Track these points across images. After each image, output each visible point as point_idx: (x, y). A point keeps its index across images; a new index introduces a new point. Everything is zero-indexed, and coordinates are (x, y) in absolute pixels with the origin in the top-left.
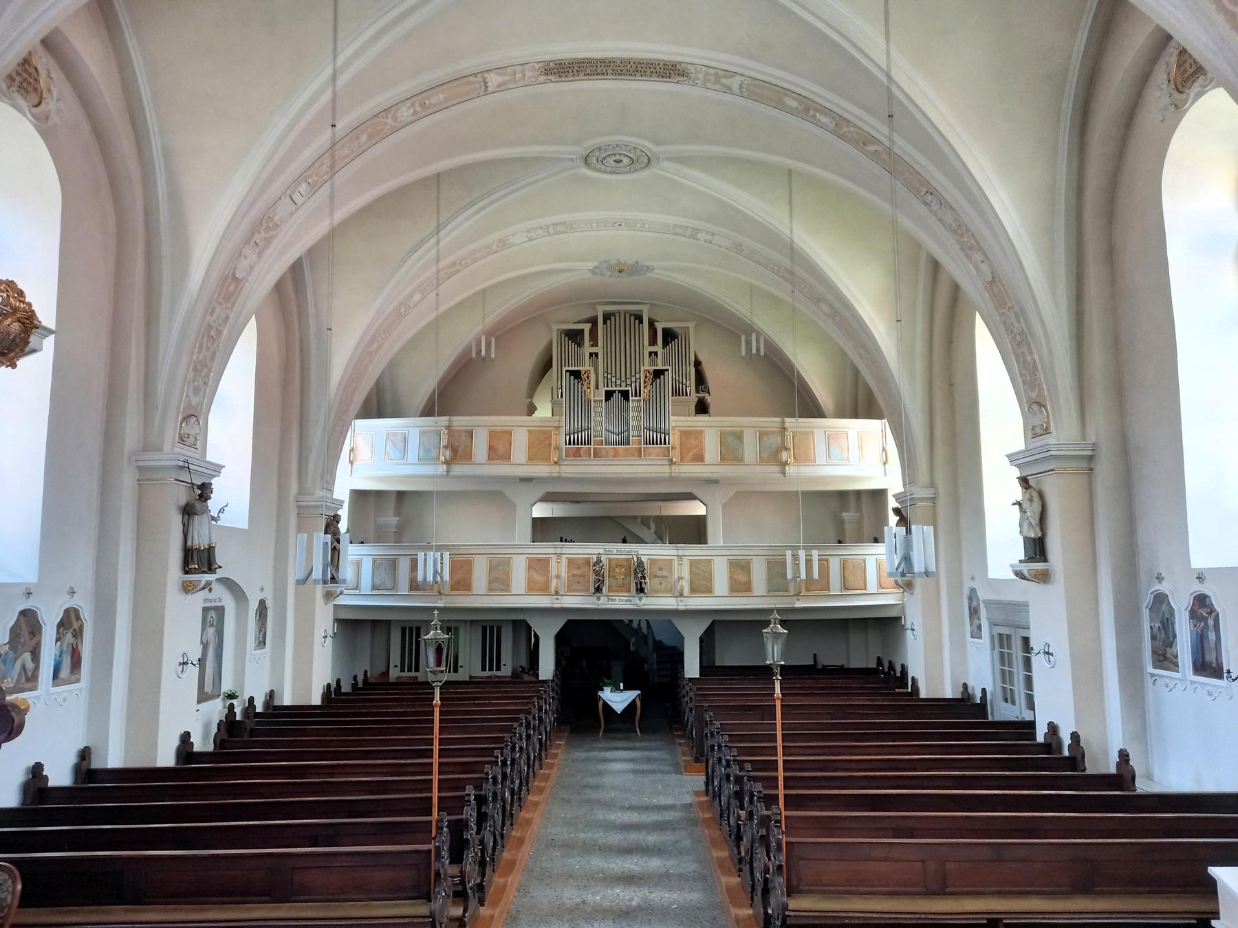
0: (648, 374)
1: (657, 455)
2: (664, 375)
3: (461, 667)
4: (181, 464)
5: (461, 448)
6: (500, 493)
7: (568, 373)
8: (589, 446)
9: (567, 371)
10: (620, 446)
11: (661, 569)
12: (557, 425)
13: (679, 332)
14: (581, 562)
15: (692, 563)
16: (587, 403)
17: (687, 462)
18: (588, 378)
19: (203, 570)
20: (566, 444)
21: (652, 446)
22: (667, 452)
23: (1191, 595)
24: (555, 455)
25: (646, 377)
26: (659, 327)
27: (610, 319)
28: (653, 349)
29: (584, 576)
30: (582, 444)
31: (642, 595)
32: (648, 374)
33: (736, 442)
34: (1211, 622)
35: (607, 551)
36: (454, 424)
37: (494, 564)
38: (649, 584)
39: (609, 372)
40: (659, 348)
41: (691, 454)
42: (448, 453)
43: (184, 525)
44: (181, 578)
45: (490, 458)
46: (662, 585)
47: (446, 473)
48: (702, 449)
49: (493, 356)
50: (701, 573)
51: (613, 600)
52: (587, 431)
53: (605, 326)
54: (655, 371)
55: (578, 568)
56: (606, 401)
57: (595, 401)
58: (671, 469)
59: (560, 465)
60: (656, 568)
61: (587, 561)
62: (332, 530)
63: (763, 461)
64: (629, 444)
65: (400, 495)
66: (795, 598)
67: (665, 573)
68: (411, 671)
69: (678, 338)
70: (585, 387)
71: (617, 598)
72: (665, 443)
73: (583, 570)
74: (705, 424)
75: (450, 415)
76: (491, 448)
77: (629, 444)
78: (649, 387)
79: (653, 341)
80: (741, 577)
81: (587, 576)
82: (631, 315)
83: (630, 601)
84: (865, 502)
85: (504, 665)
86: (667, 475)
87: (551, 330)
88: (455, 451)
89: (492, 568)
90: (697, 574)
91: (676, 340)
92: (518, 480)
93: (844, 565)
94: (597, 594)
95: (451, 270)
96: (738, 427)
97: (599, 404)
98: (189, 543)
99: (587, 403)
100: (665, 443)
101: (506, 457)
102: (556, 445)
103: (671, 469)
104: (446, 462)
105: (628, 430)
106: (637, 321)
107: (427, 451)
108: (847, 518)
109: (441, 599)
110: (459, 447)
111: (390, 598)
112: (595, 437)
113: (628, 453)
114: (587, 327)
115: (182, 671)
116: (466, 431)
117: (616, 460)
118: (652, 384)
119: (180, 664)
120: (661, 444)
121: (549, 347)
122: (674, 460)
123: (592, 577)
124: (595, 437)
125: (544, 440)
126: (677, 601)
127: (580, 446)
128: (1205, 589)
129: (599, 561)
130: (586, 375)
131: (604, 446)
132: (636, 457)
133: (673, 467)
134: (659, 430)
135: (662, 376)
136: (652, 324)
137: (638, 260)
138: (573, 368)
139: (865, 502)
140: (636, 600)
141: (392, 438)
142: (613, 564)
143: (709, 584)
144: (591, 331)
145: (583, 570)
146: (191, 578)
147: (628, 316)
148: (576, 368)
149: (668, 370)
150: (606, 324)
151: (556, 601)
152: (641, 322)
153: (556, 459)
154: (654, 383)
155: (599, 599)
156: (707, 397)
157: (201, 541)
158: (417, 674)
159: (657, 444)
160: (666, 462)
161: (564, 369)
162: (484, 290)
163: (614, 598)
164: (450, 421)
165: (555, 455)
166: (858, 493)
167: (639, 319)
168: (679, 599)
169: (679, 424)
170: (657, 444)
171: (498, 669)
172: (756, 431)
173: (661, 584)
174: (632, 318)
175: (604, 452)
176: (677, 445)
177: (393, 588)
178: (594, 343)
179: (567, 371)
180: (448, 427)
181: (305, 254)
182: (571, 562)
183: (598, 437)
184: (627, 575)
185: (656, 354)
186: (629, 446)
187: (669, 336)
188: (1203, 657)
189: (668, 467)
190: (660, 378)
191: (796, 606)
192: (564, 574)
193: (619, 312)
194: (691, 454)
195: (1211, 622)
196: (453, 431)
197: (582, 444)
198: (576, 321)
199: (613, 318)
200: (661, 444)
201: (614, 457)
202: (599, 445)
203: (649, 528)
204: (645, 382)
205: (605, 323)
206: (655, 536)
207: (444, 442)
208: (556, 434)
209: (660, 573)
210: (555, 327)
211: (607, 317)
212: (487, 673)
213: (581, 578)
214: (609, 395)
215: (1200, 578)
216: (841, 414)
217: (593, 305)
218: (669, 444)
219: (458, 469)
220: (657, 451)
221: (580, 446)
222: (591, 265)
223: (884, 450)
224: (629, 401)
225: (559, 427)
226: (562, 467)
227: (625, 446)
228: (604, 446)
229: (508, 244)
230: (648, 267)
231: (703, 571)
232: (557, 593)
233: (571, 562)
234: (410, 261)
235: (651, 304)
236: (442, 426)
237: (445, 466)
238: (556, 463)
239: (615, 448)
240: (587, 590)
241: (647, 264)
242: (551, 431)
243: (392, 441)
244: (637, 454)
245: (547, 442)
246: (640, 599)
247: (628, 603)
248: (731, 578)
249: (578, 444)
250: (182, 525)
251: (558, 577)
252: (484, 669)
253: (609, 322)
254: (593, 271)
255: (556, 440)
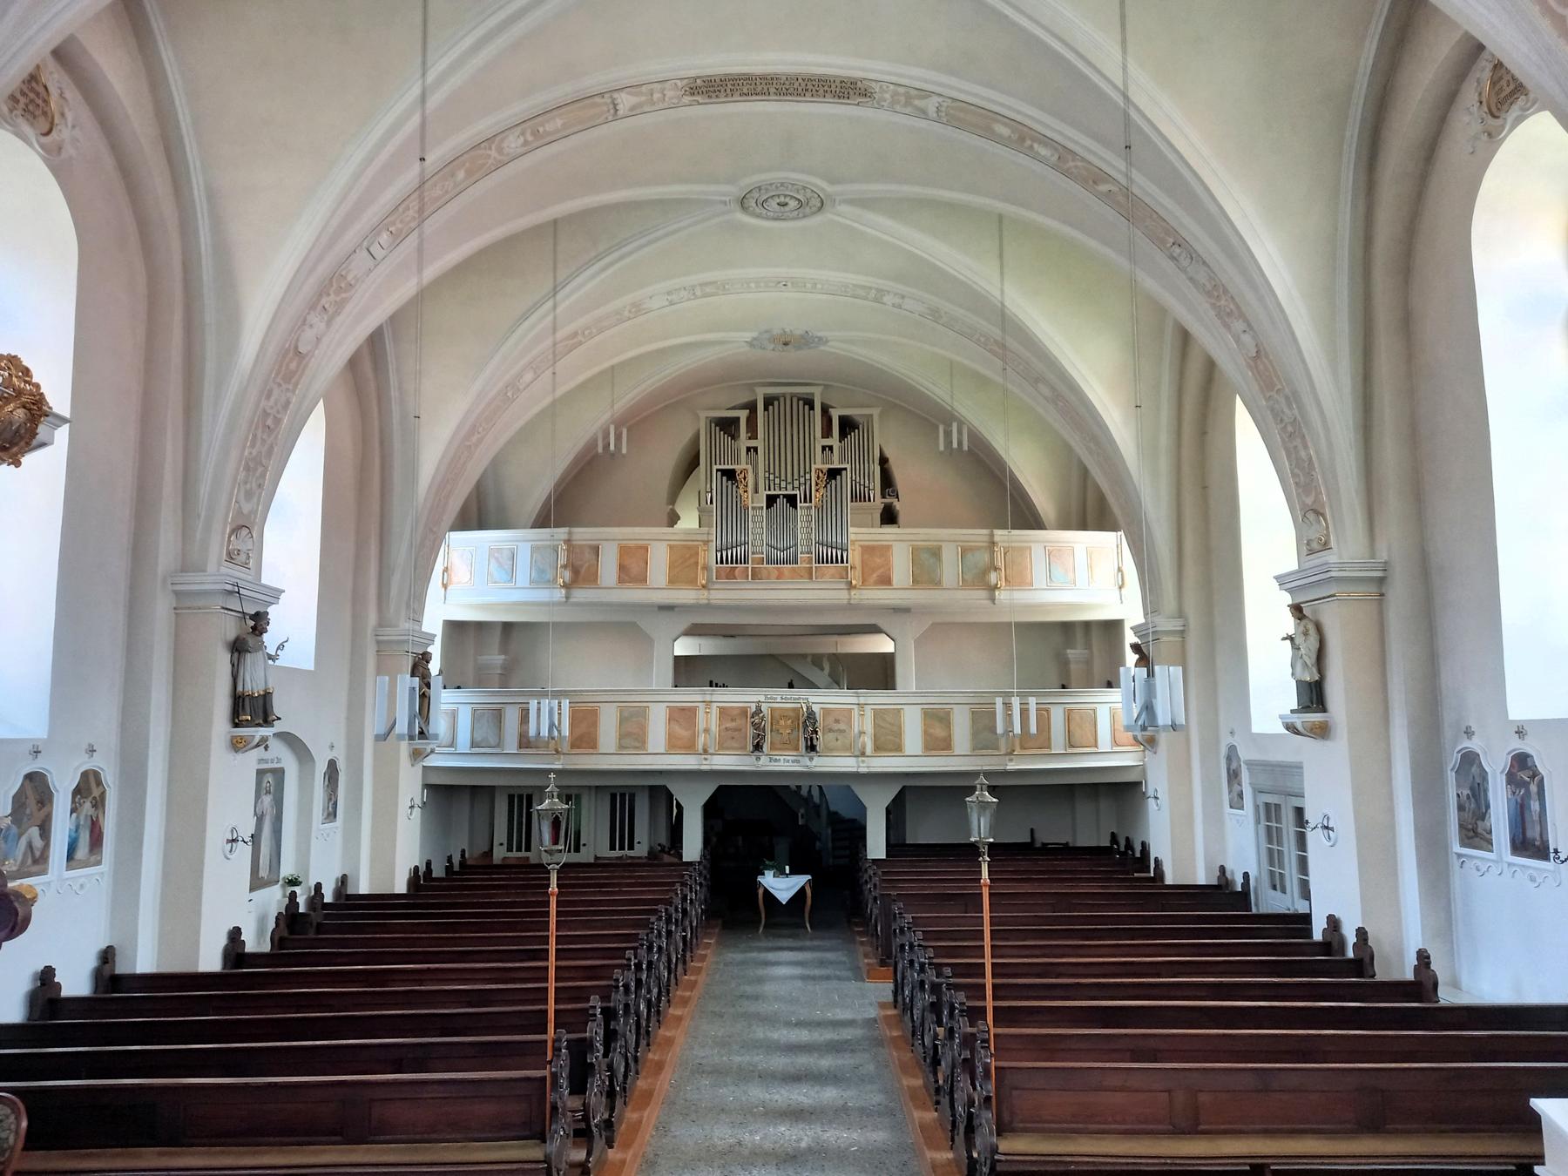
0: (821, 474)
1: (833, 577)
2: (841, 475)
3: (584, 845)
4: (229, 587)
5: (584, 568)
6: (634, 624)
7: (719, 473)
8: (746, 565)
9: (718, 470)
10: (785, 565)
11: (837, 721)
12: (706, 539)
13: (860, 420)
14: (736, 712)
15: (876, 713)
16: (743, 511)
17: (870, 585)
18: (745, 478)
19: (257, 722)
20: (717, 563)
21: (825, 565)
22: (844, 573)
23: (1509, 753)
24: (703, 576)
25: (818, 478)
26: (835, 414)
27: (773, 405)
28: (827, 442)
29: (740, 730)
30: (737, 563)
31: (813, 754)
32: (821, 474)
33: (932, 560)
34: (1533, 788)
35: (769, 699)
36: (575, 537)
37: (626, 714)
38: (821, 741)
39: (772, 471)
40: (834, 441)
41: (875, 575)
42: (567, 575)
43: (233, 665)
44: (229, 732)
45: (621, 580)
46: (839, 742)
47: (564, 599)
48: (890, 569)
49: (624, 451)
50: (888, 726)
51: (776, 760)
52: (743, 547)
53: (766, 413)
54: (830, 470)
55: (732, 720)
56: (767, 508)
57: (753, 508)
58: (850, 594)
59: (709, 589)
60: (830, 720)
61: (744, 711)
62: (421, 671)
63: (966, 584)
64: (796, 563)
65: (507, 627)
66: (1007, 758)
67: (842, 726)
68: (521, 851)
69: (858, 429)
70: (741, 491)
71: (782, 758)
72: (842, 562)
73: (739, 723)
74: (893, 537)
75: (570, 526)
76: (622, 568)
77: (796, 563)
78: (822, 491)
79: (827, 433)
80: (939, 732)
81: (743, 730)
82: (799, 399)
83: (798, 761)
84: (1095, 636)
85: (639, 843)
86: (845, 602)
87: (698, 418)
88: (576, 572)
89: (623, 720)
90: (882, 727)
91: (856, 431)
92: (656, 609)
93: (1069, 716)
94: (756, 753)
95: (571, 342)
96: (935, 541)
97: (758, 512)
98: (240, 688)
99: (743, 511)
100: (842, 562)
101: (641, 579)
102: (705, 564)
103: (850, 594)
104: (565, 586)
105: (796, 545)
106: (807, 407)
107: (541, 571)
108: (1073, 656)
109: (559, 759)
110: (582, 566)
111: (494, 758)
112: (753, 553)
113: (795, 574)
114: (743, 415)
115: (231, 851)
116: (591, 547)
117: (781, 583)
118: (826, 486)
119: (228, 841)
120: (837, 562)
121: (696, 440)
122: (854, 582)
123: (750, 731)
124: (753, 553)
125: (690, 558)
126: (857, 762)
127: (735, 565)
128: (1526, 747)
129: (759, 711)
130: (742, 475)
131: (765, 565)
132: (805, 579)
133: (853, 592)
134: (834, 545)
135: (838, 477)
136: (825, 410)
137: (808, 330)
138: (726, 467)
139: (1095, 636)
140: (806, 761)
141: (496, 555)
142: (777, 715)
143: (897, 740)
144: (748, 420)
145: (739, 723)
146: (242, 732)
147: (795, 400)
148: (730, 467)
149: (846, 469)
150: (768, 410)
151: (704, 762)
152: (812, 408)
153: (704, 582)
154: (829, 486)
155: (758, 758)
156: (896, 503)
157: (254, 686)
158: (528, 854)
159: (832, 562)
160: (843, 586)
161: (715, 468)
162: (613, 367)
163: (778, 758)
164: (570, 533)
165: (703, 576)
166: (1087, 625)
167: (810, 404)
168: (860, 759)
169: (860, 537)
170: (832, 562)
171: (631, 847)
172: (957, 546)
173: (837, 740)
174: (801, 403)
175: (765, 573)
176: (858, 563)
177: (498, 746)
178: (753, 434)
179: (718, 470)
180: (568, 542)
181: (386, 322)
182: (723, 712)
183: (757, 553)
184: (794, 728)
185: (831, 448)
186: (797, 566)
187: (848, 426)
188: (1524, 833)
189: (846, 592)
190: (835, 479)
191: (1008, 768)
192: (714, 728)
193: (784, 395)
194: (875, 575)
195: (1533, 788)
196: (574, 546)
197: (737, 563)
198: (729, 407)
199: (776, 403)
200: (837, 562)
201: (777, 579)
202: (758, 564)
203: (822, 669)
204: (817, 484)
205: (766, 409)
206: (829, 679)
207: (562, 560)
208: (705, 551)
209: (836, 727)
210: (703, 415)
211: (769, 402)
212: (617, 853)
213: (736, 733)
214: (771, 500)
215: (1520, 732)
216: (1065, 525)
217: (751, 387)
218: (847, 562)
219: (581, 595)
220: (832, 571)
221: (735, 565)
222: (748, 336)
223: (1119, 570)
224: (796, 508)
225: (708, 541)
226: (711, 591)
227: (792, 566)
228: (765, 565)
229: (644, 309)
230: (820, 339)
231: (890, 724)
232: (705, 751)
233: (723, 712)
234: (520, 331)
235: (824, 385)
236: (560, 540)
237: (563, 591)
238: (704, 587)
239: (779, 568)
240: (744, 748)
241: (819, 334)
242: (697, 547)
243: (497, 559)
244: (806, 575)
245: (692, 560)
246: (811, 759)
247: (795, 764)
248: (926, 733)
249: (732, 563)
250: (230, 666)
251: (707, 731)
252: (612, 848)
253: (771, 407)
254: (751, 344)
255: (704, 558)
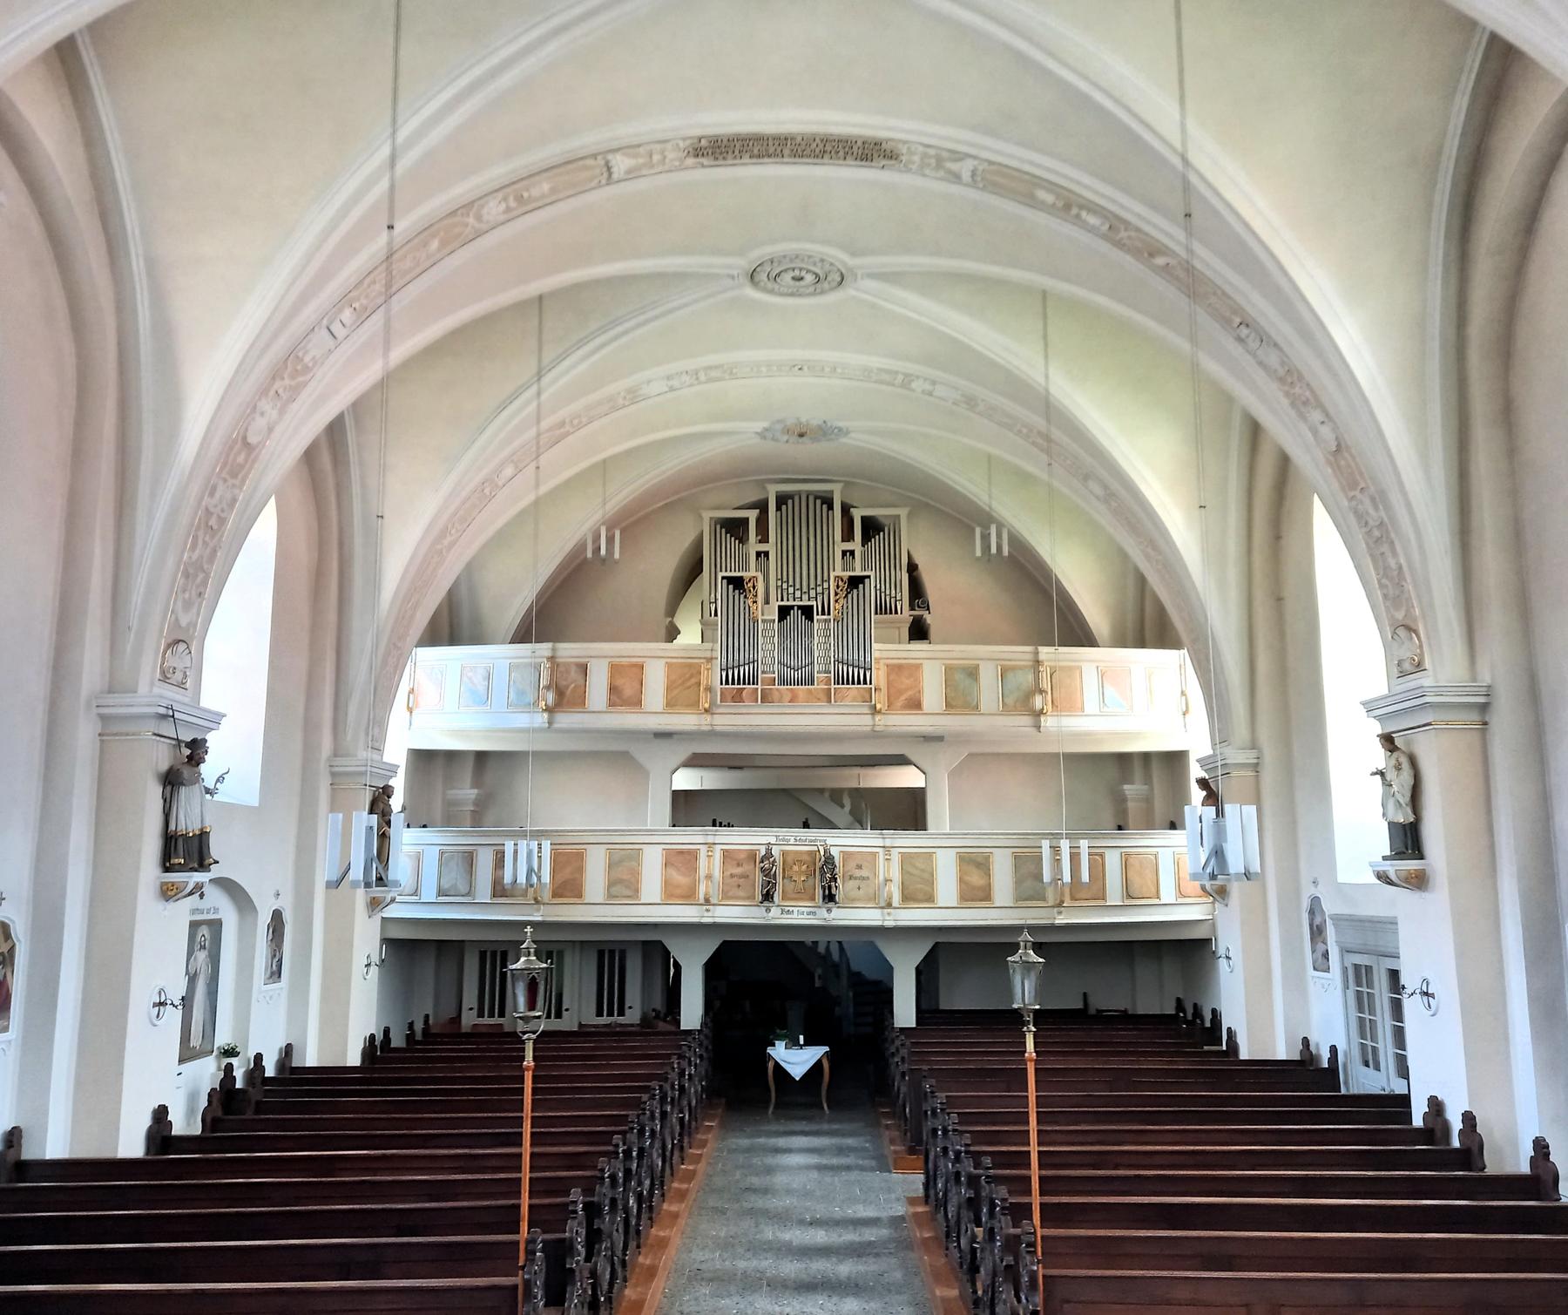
0: (840, 583)
8: (755, 686)
9: (723, 578)
11: (859, 867)
13: (885, 521)
18: (754, 587)
20: (722, 684)
24: (706, 697)
25: (838, 587)
26: (857, 515)
28: (848, 546)
31: (831, 905)
32: (840, 583)
36: (559, 653)
40: (856, 545)
41: (903, 698)
42: (550, 697)
43: (165, 801)
45: (611, 704)
47: (547, 725)
49: (617, 556)
52: (800, 671)
53: (779, 513)
55: (738, 865)
56: (779, 621)
57: (763, 621)
59: (713, 714)
61: (752, 855)
63: (1007, 709)
64: (813, 684)
65: (481, 757)
67: (864, 873)
70: (750, 601)
71: (795, 909)
72: (865, 683)
73: (747, 868)
77: (813, 684)
78: (842, 601)
79: (848, 535)
80: (976, 879)
82: (816, 498)
83: (814, 913)
84: (1155, 767)
86: (869, 729)
88: (560, 693)
89: (611, 866)
94: (766, 904)
98: (172, 827)
101: (636, 702)
103: (874, 719)
105: (812, 663)
106: (825, 506)
107: (521, 693)
109: (538, 910)
110: (567, 687)
112: (763, 672)
114: (752, 515)
118: (846, 596)
122: (878, 706)
123: (759, 878)
124: (763, 672)
126: (883, 914)
127: (741, 686)
129: (769, 854)
130: (750, 585)
133: (878, 718)
134: (856, 663)
135: (861, 586)
136: (846, 510)
140: (823, 913)
142: (789, 859)
144: (758, 520)
145: (747, 868)
147: (811, 499)
149: (869, 577)
150: (781, 510)
151: (706, 914)
152: (831, 507)
153: (707, 706)
159: (853, 683)
160: (866, 710)
162: (604, 461)
163: (791, 909)
164: (554, 650)
166: (1146, 757)
167: (828, 502)
169: (885, 654)
171: (621, 1013)
173: (859, 888)
175: (776, 695)
176: (883, 684)
177: (468, 894)
178: (764, 539)
179: (723, 578)
182: (727, 855)
185: (852, 553)
187: (872, 528)
189: (870, 716)
190: (857, 588)
192: (717, 873)
193: (799, 493)
194: (903, 698)
199: (790, 502)
200: (859, 683)
203: (842, 806)
204: (836, 594)
205: (778, 508)
208: (708, 669)
209: (858, 873)
210: (707, 515)
212: (605, 1020)
214: (784, 612)
216: (1121, 641)
217: (761, 484)
218: (871, 684)
219: (565, 720)
221: (741, 686)
222: (759, 426)
224: (812, 621)
232: (707, 901)
233: (727, 855)
237: (546, 715)
238: (706, 711)
240: (752, 897)
241: (840, 424)
244: (822, 696)
245: (693, 680)
248: (961, 880)
250: (162, 801)
251: (709, 877)
252: (599, 1014)
253: (784, 507)
